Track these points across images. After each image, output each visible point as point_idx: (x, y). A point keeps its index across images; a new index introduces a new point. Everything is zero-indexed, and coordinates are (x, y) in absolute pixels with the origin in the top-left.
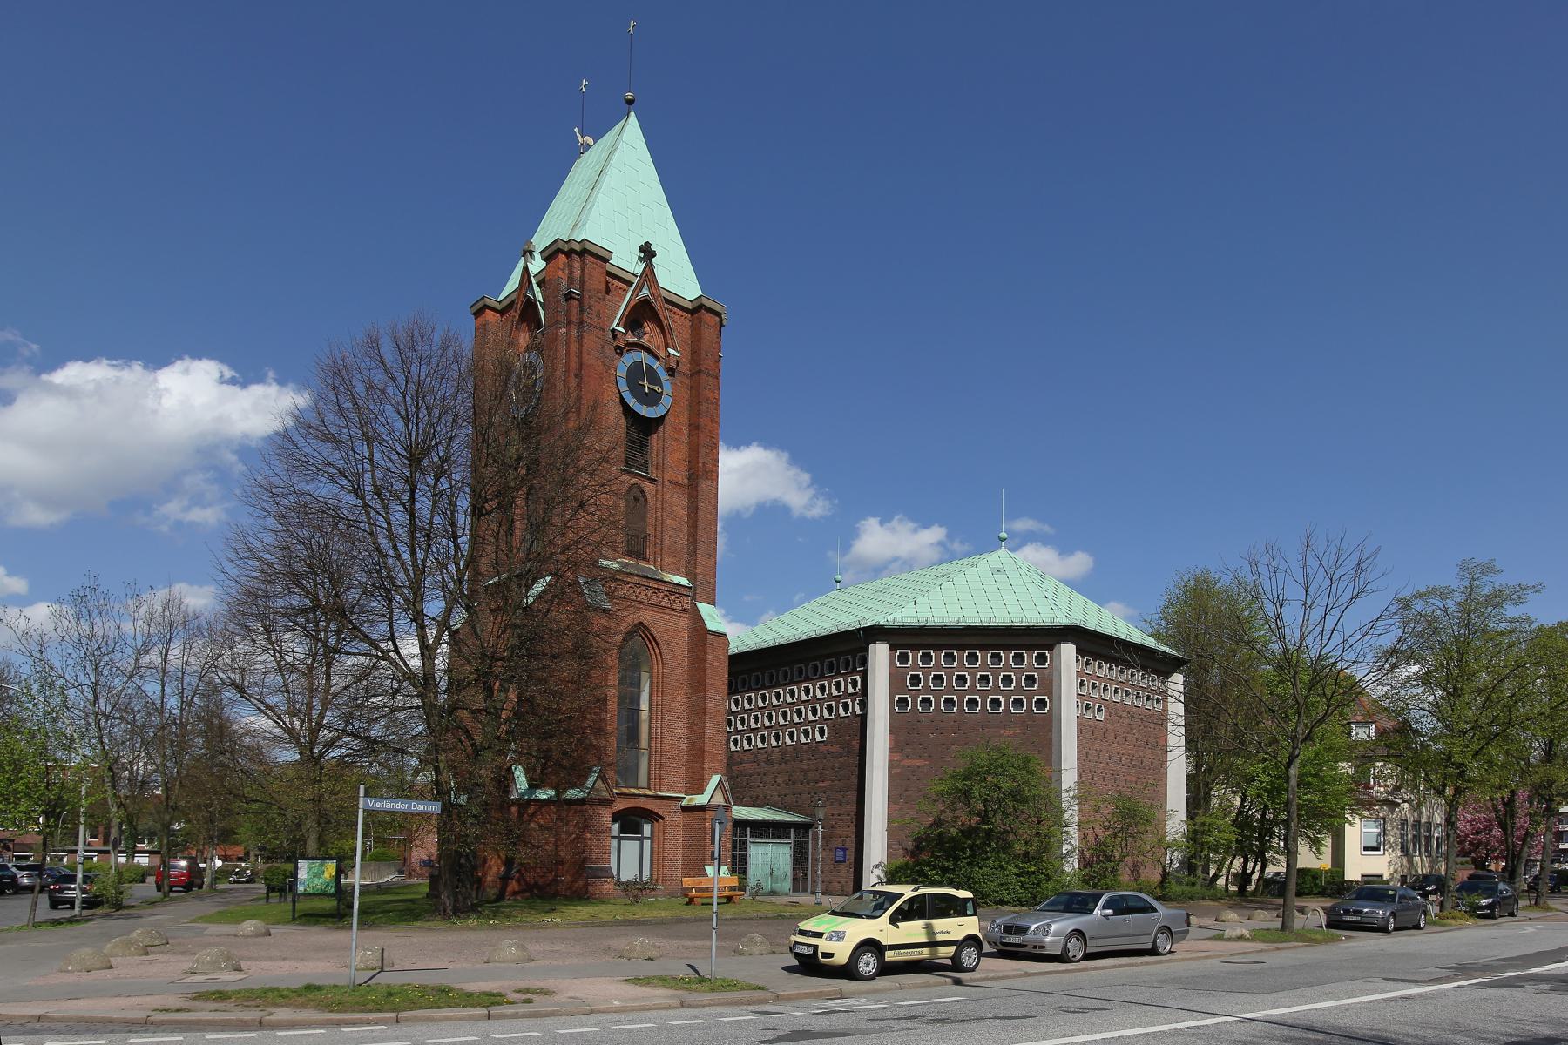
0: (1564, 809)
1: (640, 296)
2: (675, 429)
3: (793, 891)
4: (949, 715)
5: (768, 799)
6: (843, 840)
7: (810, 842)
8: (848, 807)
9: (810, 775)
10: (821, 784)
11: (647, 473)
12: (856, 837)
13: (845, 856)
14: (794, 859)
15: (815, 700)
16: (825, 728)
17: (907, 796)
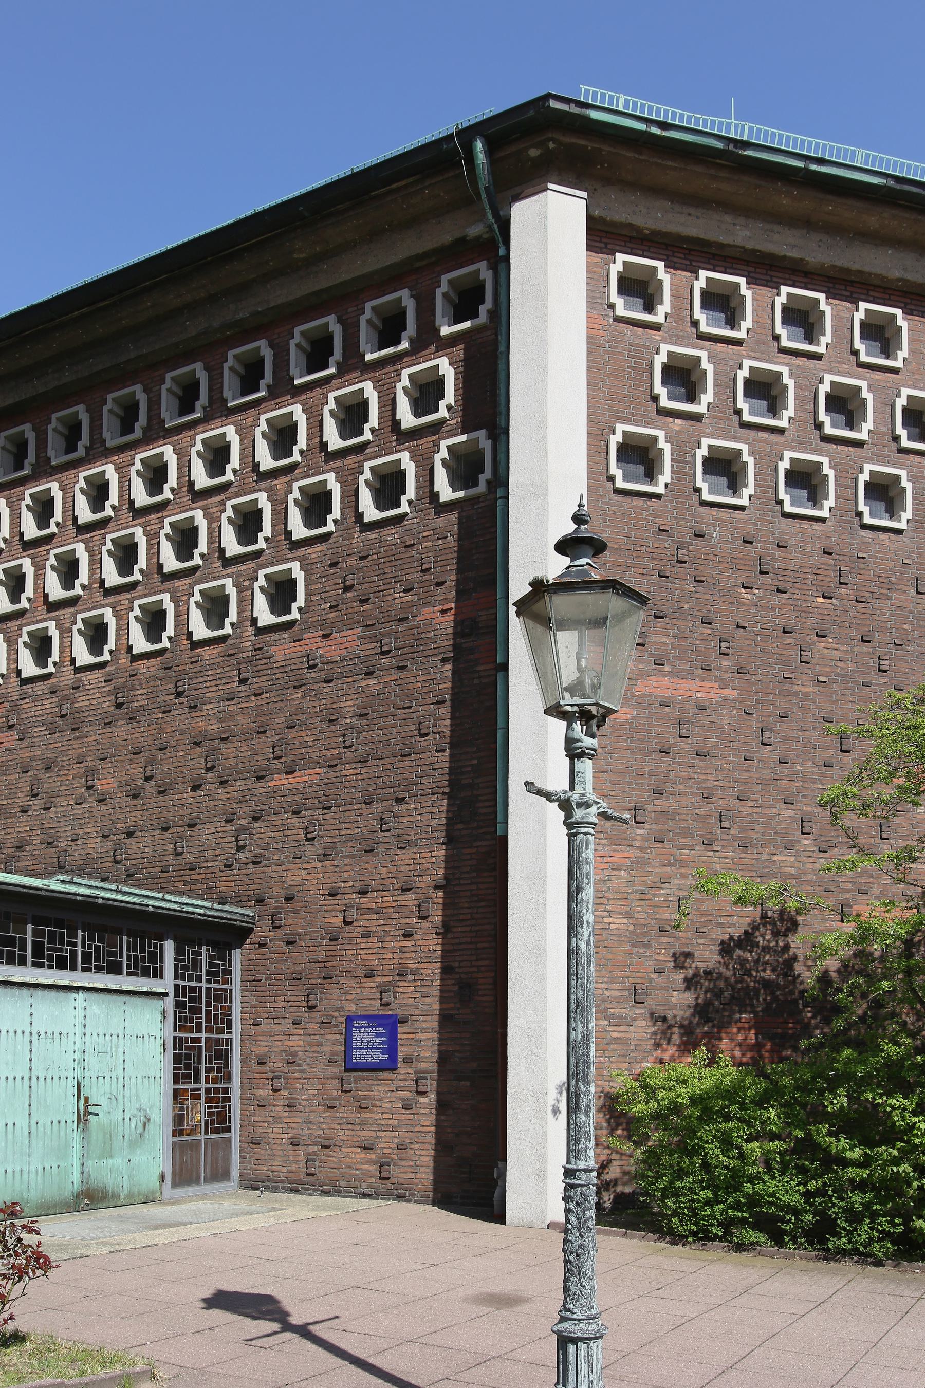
3: (174, 1185)
4: (806, 525)
5: (63, 852)
6: (383, 989)
7: (237, 995)
8: (405, 857)
10: (279, 781)
12: (446, 970)
13: (392, 1048)
14: (177, 1059)
15: (126, 516)
16: (299, 575)
17: (662, 816)
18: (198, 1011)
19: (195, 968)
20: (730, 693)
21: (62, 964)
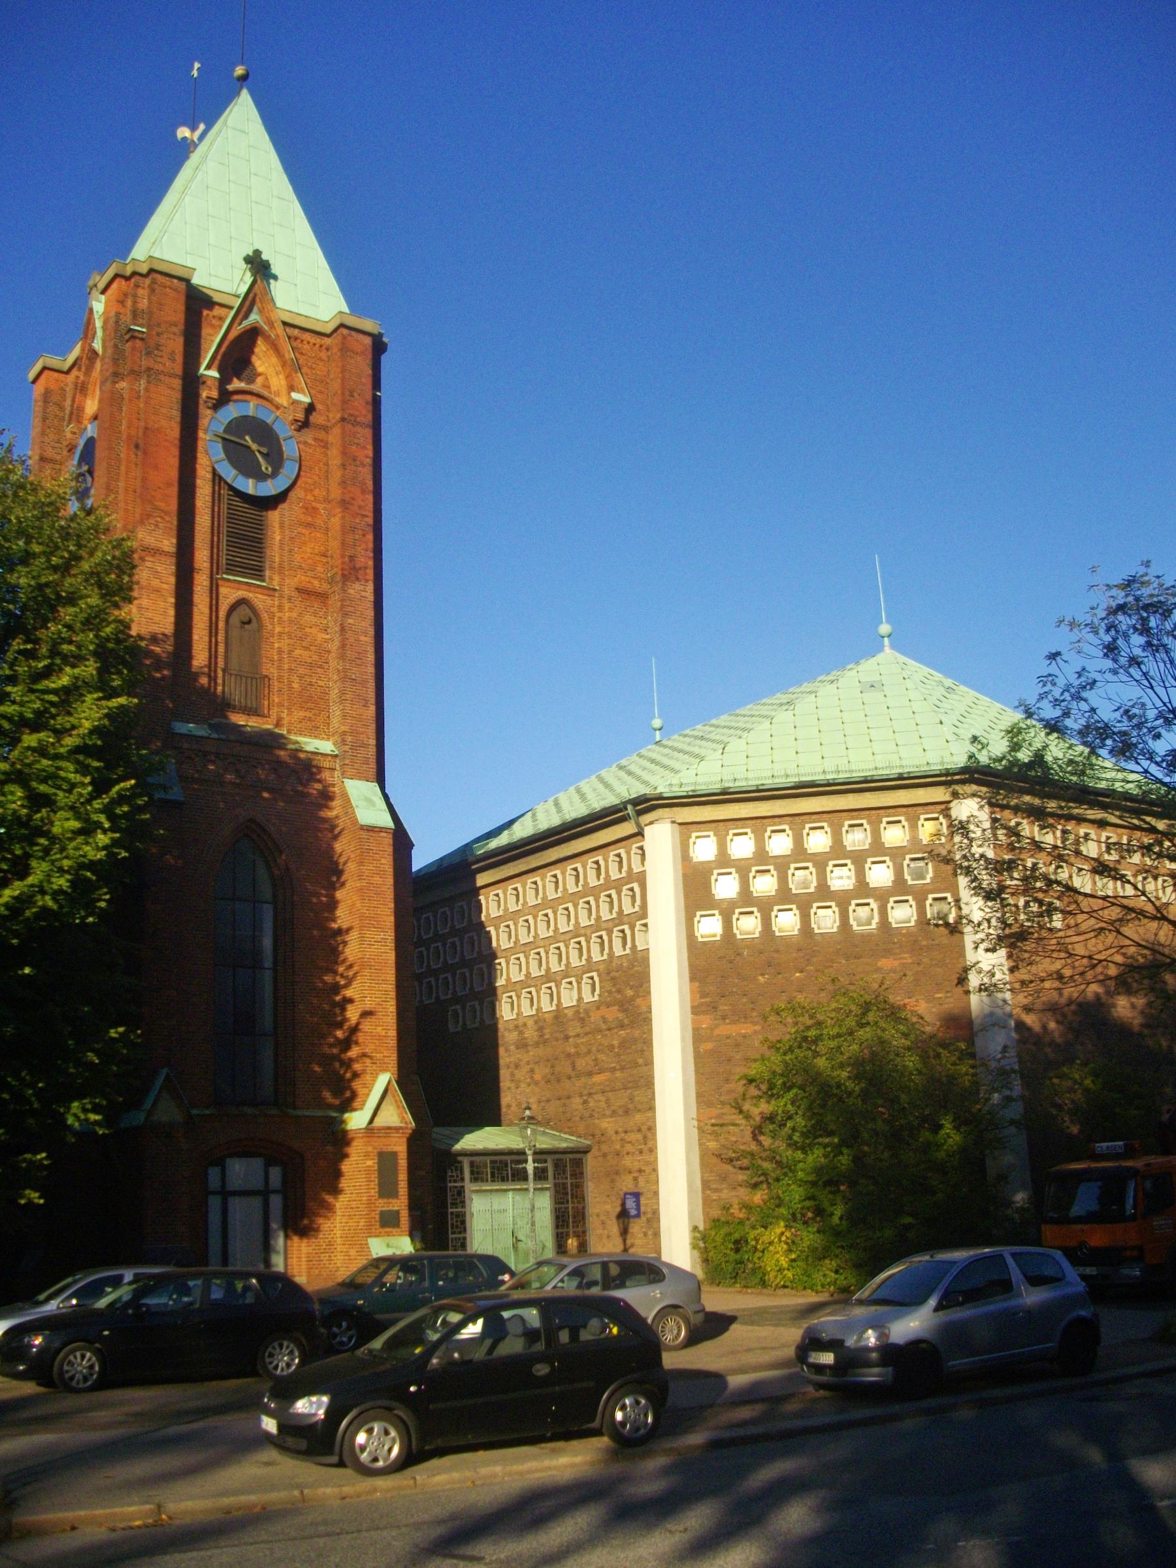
0: (2, 831)
1: (245, 323)
2: (306, 508)
9: (581, 1064)
11: (263, 581)
14: (557, 1217)
18: (567, 1194)
19: (564, 1173)
20: (758, 1028)
21: (503, 1180)
